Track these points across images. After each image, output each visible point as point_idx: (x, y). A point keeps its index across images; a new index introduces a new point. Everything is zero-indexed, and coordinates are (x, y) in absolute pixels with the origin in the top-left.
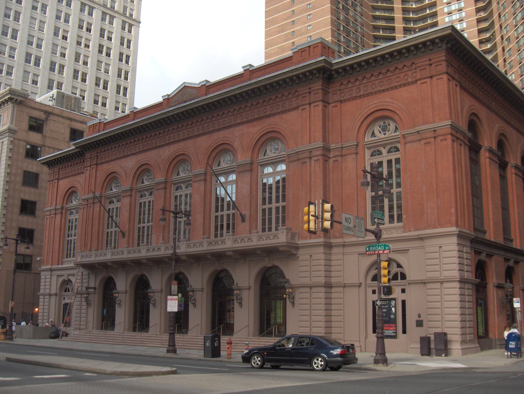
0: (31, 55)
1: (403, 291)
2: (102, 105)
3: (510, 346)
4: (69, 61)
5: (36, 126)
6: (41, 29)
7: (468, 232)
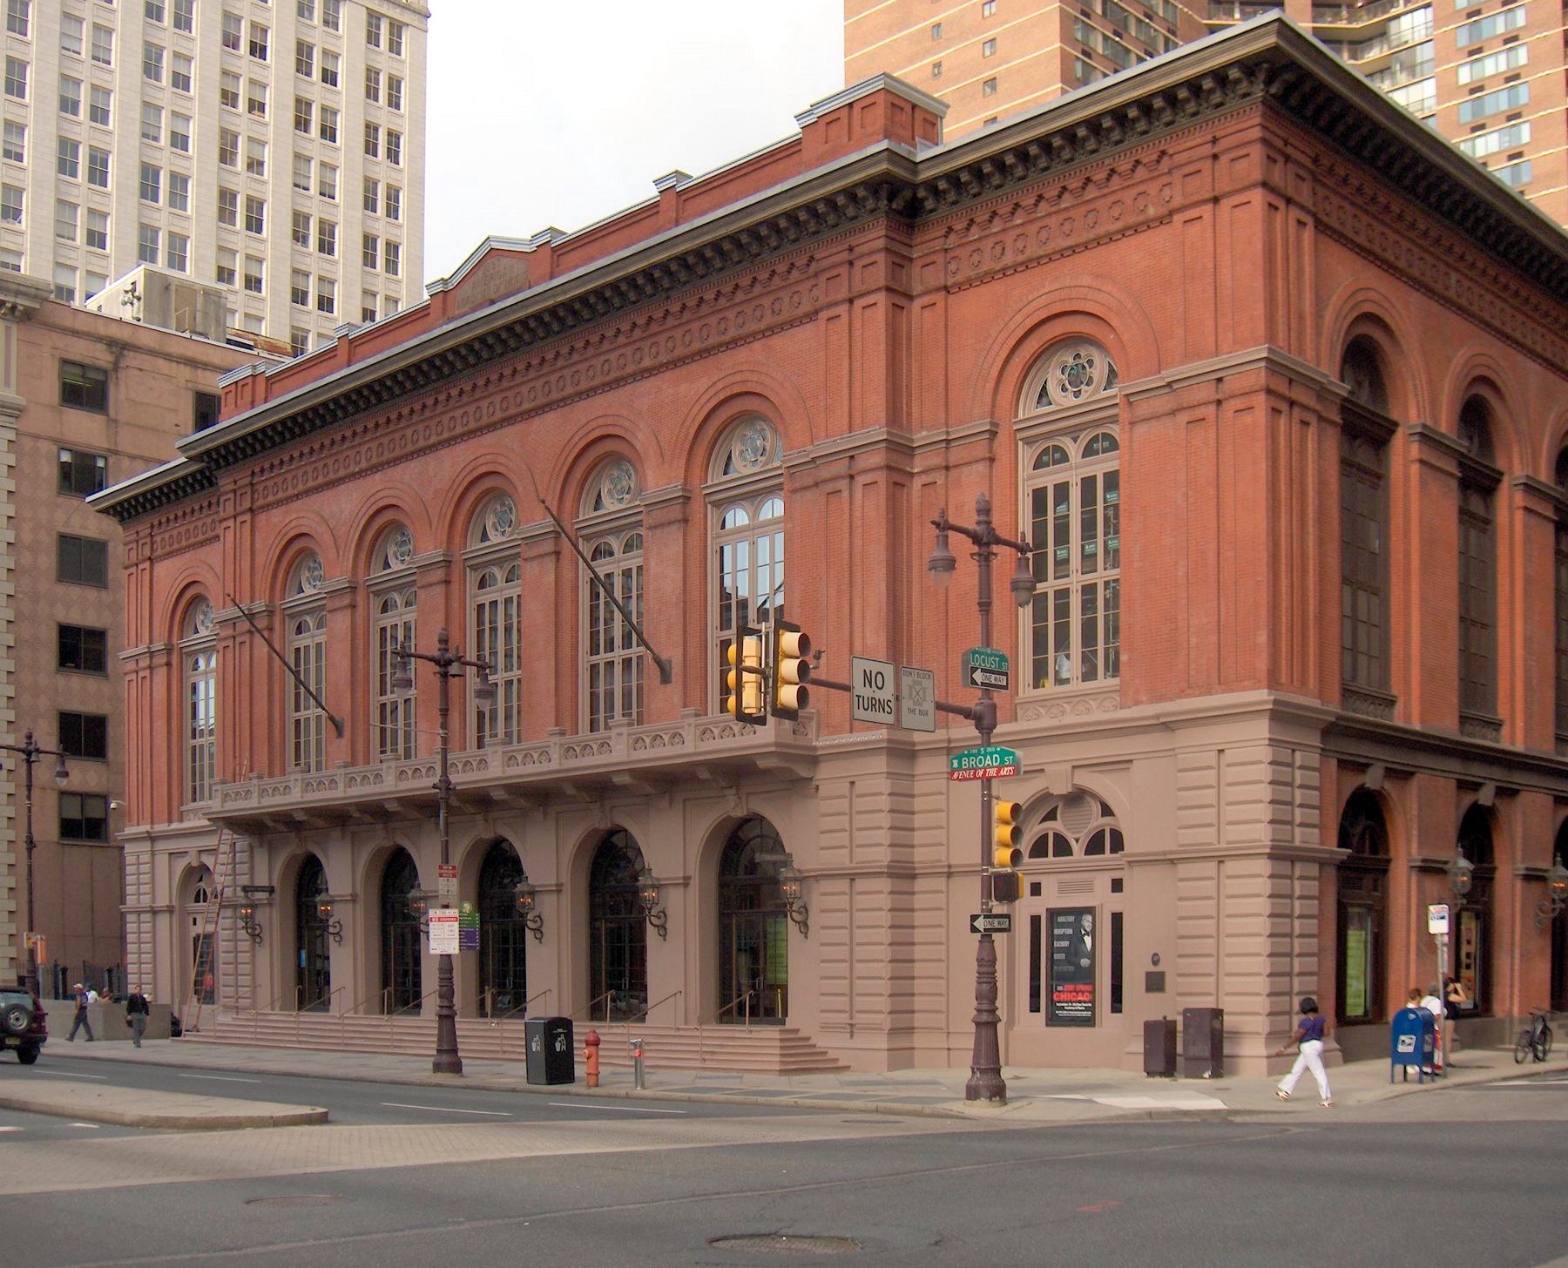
0: (76, 145)
1: (1117, 886)
2: (321, 307)
3: (1401, 1049)
4: (199, 162)
5: (85, 390)
6: (101, 57)
7: (1316, 703)
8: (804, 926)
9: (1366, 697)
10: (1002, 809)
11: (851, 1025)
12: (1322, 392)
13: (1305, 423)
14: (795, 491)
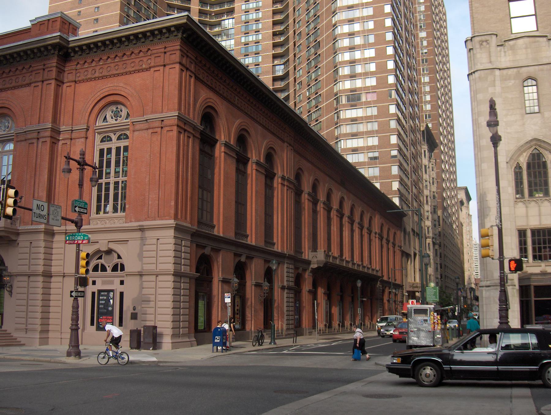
1: (122, 283)
3: (216, 341)
7: (189, 225)
8: (11, 292)
9: (205, 225)
10: (83, 255)
11: (26, 329)
12: (195, 128)
13: (189, 137)
14: (17, 142)
